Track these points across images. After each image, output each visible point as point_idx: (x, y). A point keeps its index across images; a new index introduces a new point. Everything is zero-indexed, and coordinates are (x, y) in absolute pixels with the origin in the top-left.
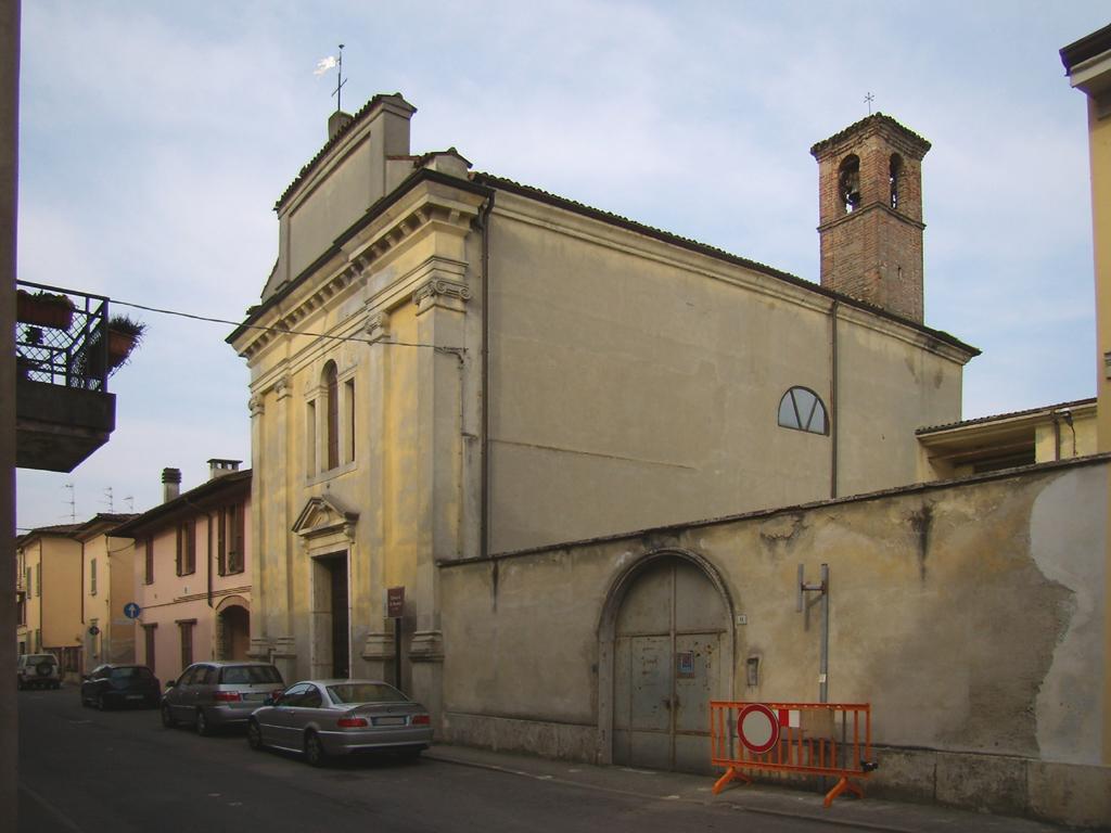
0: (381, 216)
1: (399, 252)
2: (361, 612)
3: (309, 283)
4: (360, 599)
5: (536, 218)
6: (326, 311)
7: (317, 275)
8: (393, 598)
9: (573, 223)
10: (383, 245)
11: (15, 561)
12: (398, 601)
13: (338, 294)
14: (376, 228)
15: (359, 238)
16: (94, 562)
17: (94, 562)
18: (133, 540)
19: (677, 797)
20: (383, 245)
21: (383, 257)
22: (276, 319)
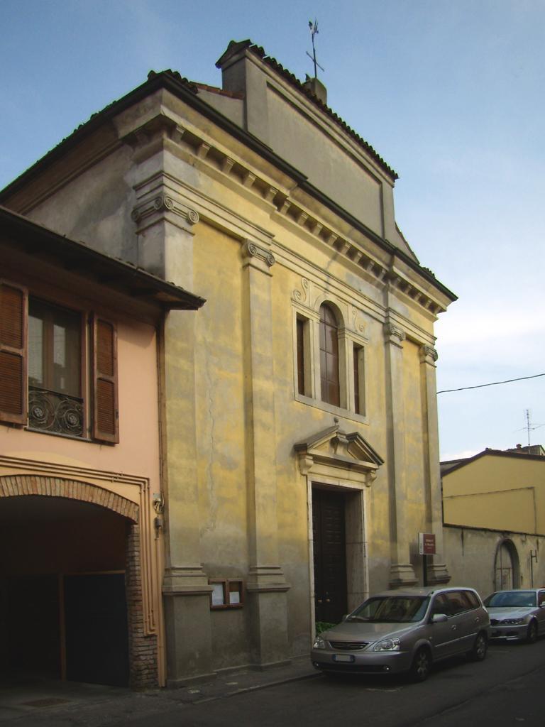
0: (427, 282)
1: (414, 306)
2: (375, 547)
3: (347, 227)
4: (374, 536)
5: (152, 590)
6: (335, 258)
7: (358, 234)
8: (427, 540)
9: (336, 131)
10: (413, 292)
11: (524, 447)
12: (427, 543)
13: (355, 263)
14: (419, 281)
15: (409, 270)
16: (358, 349)
17: (358, 349)
18: (522, 447)
19: (523, 720)
20: (413, 292)
21: (406, 296)
22: (285, 192)
